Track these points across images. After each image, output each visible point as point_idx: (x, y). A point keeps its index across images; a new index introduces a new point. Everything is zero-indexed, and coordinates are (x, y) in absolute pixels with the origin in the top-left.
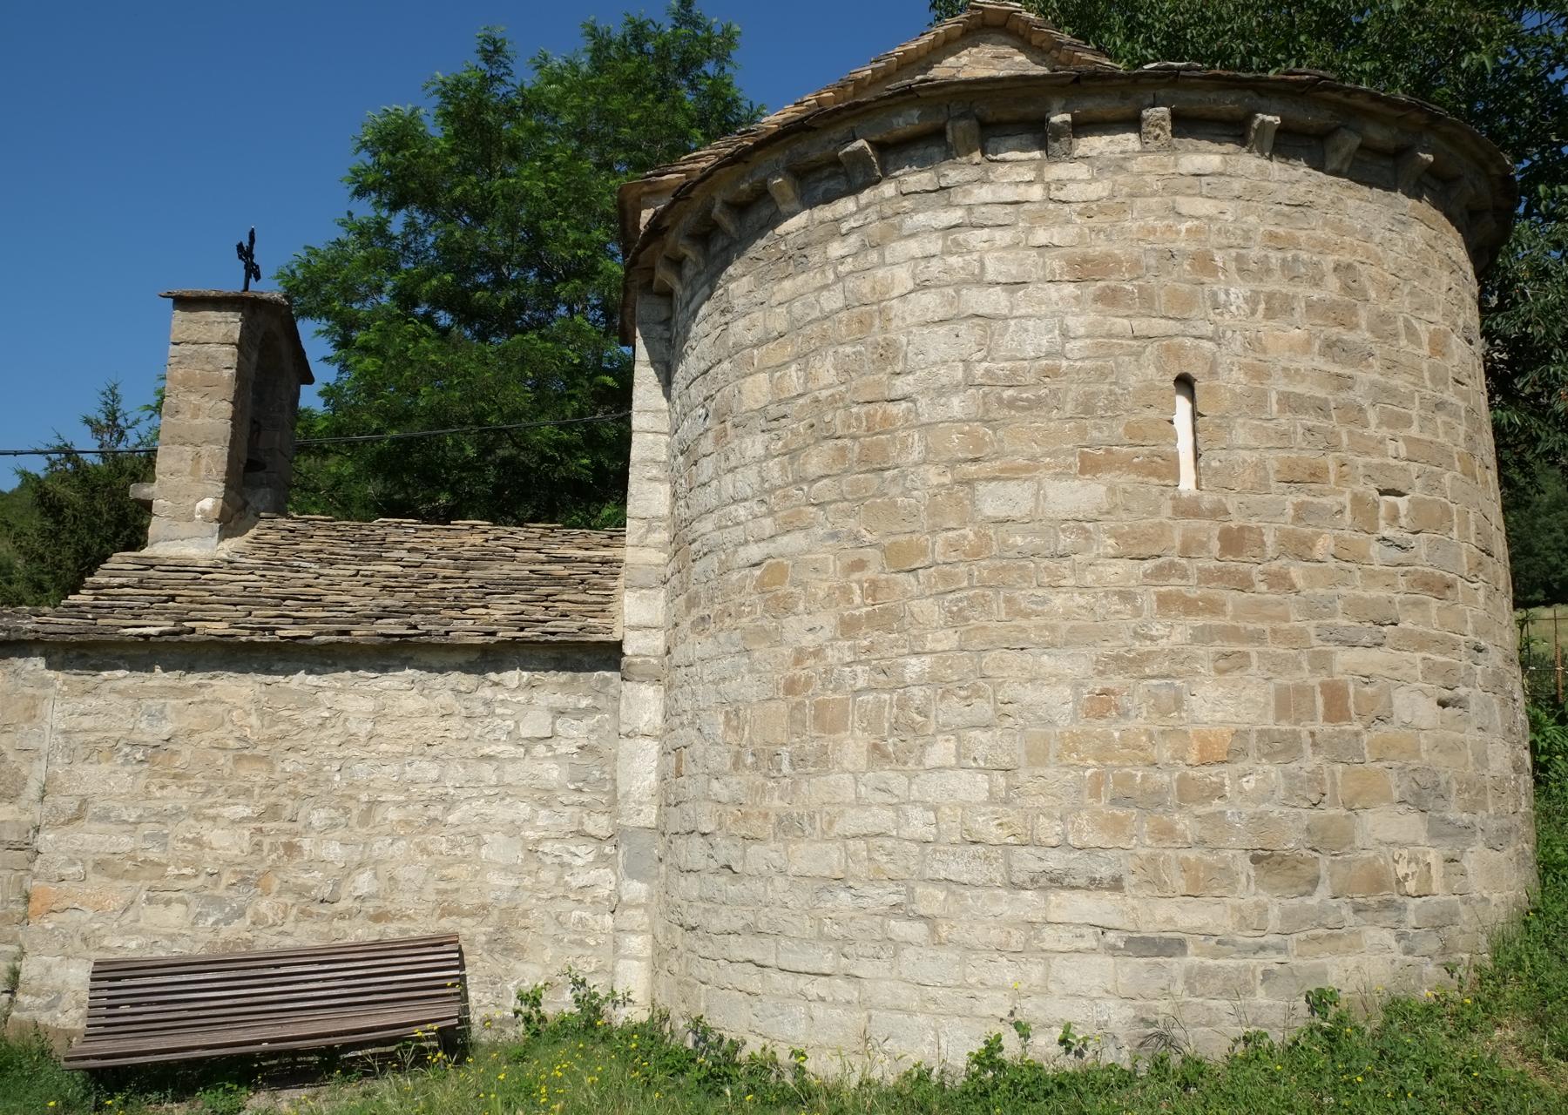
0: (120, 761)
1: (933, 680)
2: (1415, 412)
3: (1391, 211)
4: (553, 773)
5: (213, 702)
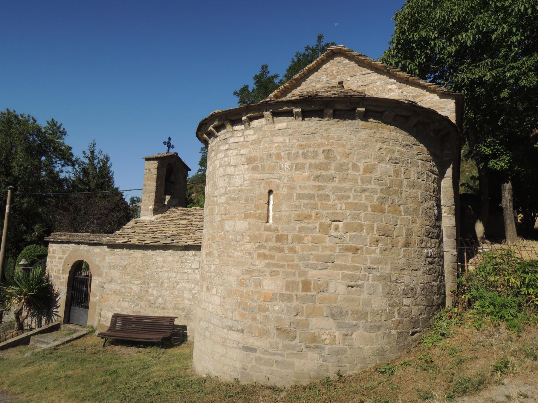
2: (352, 194)
3: (352, 128)
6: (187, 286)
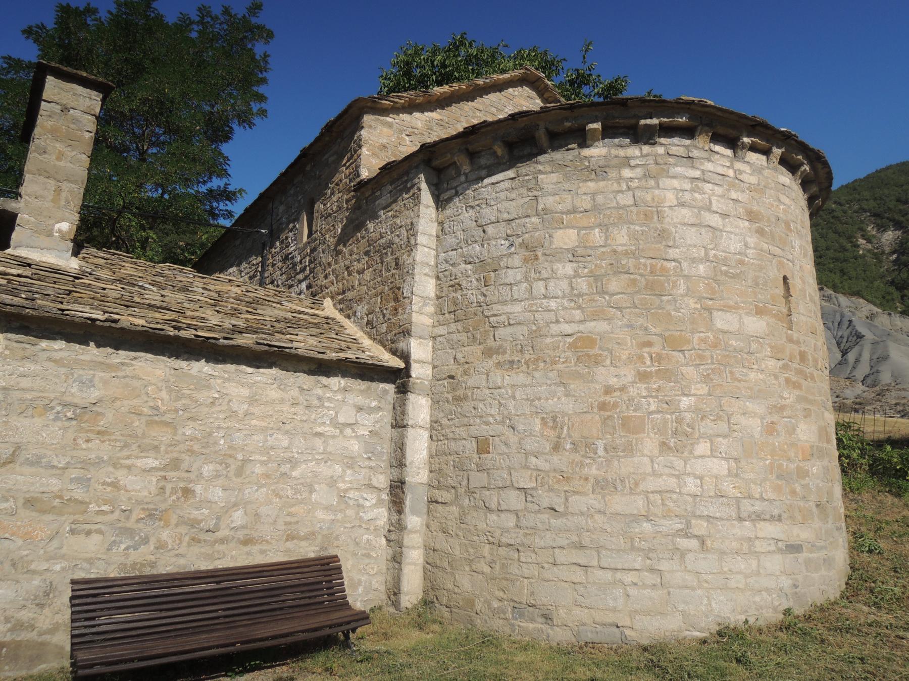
0: (52, 417)
1: (696, 410)
4: (355, 447)
5: (132, 377)
6: (325, 470)
